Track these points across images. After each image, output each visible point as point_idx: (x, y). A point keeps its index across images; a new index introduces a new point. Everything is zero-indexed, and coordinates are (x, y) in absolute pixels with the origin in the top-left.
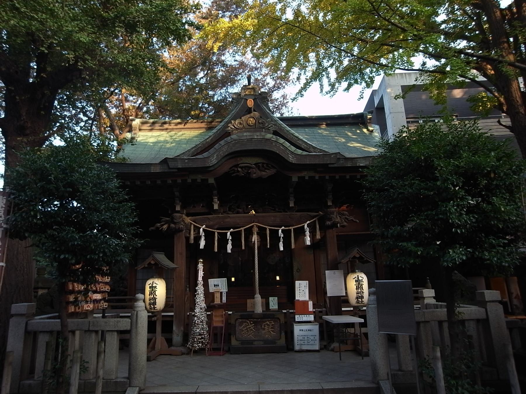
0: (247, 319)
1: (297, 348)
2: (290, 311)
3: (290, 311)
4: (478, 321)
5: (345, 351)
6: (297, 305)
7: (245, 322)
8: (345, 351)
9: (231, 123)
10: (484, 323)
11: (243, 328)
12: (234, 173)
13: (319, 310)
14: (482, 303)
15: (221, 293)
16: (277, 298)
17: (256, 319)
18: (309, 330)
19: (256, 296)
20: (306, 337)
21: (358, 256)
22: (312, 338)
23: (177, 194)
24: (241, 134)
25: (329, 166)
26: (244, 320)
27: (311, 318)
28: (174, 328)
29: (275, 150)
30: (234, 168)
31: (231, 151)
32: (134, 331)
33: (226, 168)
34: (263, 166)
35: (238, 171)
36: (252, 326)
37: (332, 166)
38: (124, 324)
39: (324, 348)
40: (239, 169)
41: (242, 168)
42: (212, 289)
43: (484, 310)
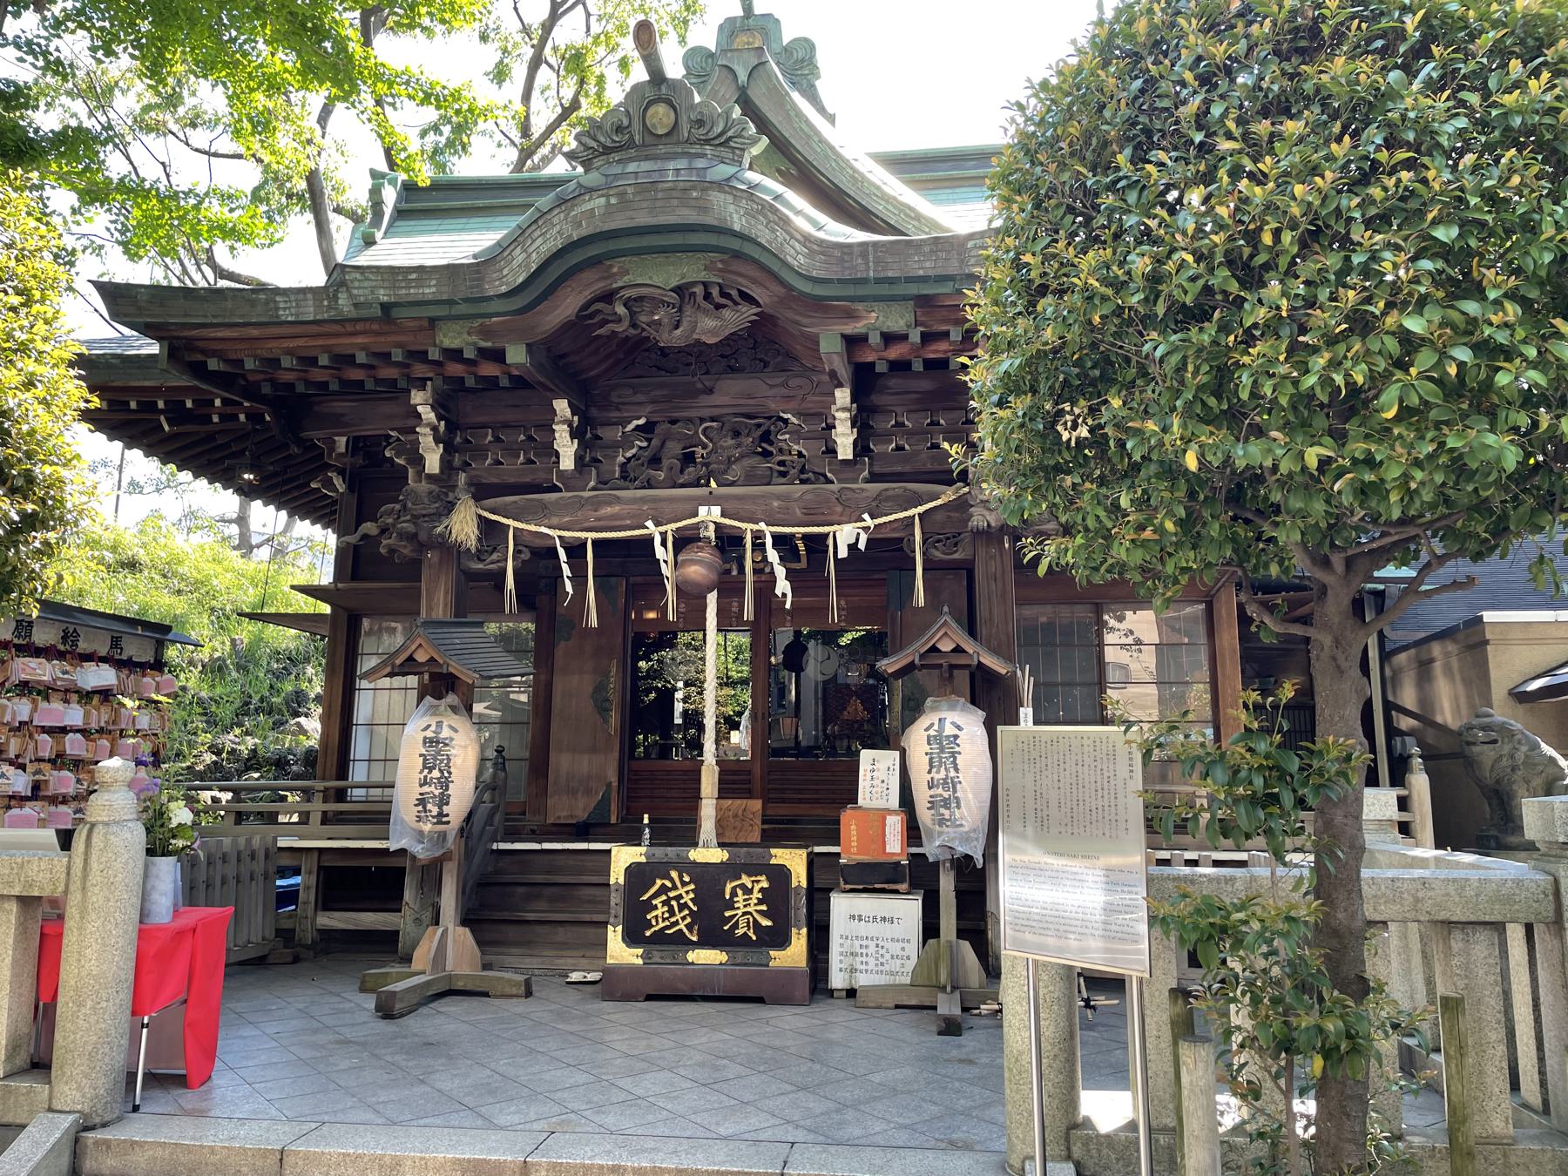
5: (897, 1007)
8: (897, 1007)
11: (655, 896)
18: (883, 919)
20: (872, 945)
22: (895, 948)
24: (617, 169)
34: (707, 296)
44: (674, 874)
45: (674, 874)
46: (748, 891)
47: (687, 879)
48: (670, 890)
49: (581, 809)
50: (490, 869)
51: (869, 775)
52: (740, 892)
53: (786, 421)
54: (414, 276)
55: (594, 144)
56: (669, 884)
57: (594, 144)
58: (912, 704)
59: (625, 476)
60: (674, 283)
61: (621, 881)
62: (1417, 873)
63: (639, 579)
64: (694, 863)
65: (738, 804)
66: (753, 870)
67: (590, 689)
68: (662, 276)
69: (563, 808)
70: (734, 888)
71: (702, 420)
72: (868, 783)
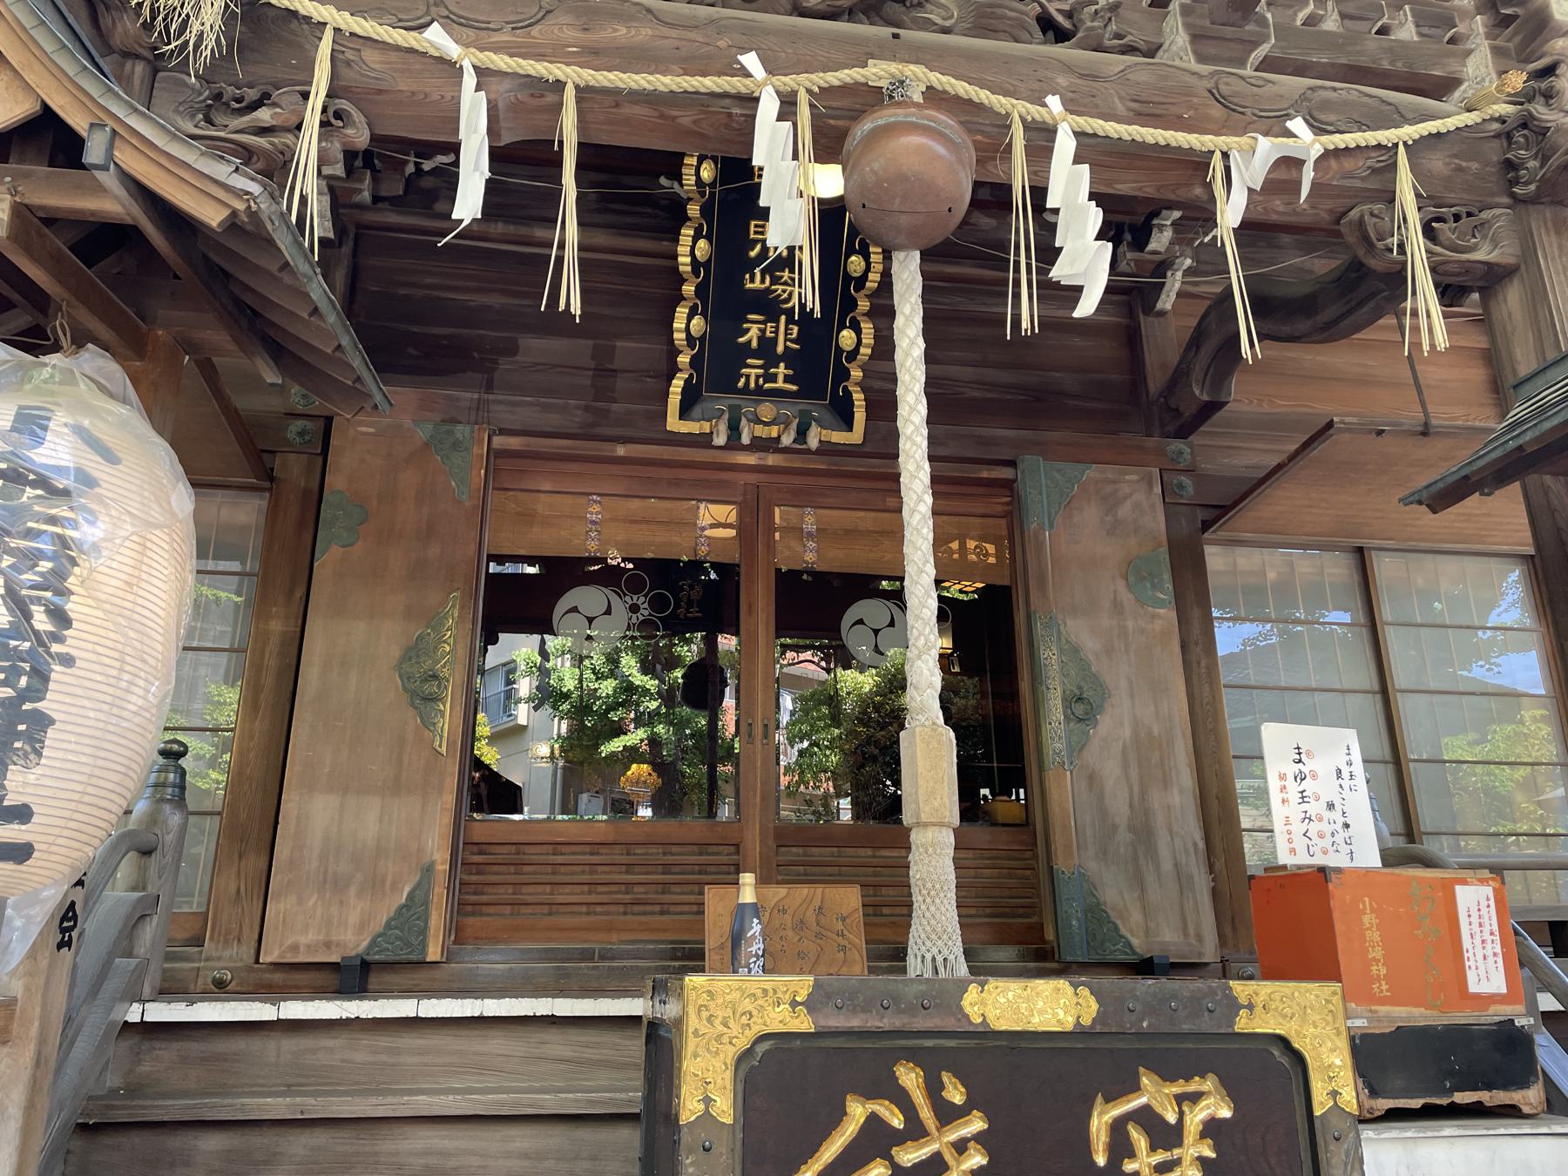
44: (910, 1078)
45: (910, 1078)
46: (1165, 1135)
47: (955, 1094)
48: (901, 1138)
49: (352, 930)
50: (113, 1080)
51: (1293, 788)
52: (1139, 1139)
56: (897, 1122)
58: (1079, 709)
61: (724, 1108)
63: (514, 443)
64: (986, 1034)
66: (1178, 1059)
67: (396, 652)
69: (304, 925)
70: (1118, 1128)
72: (1295, 811)
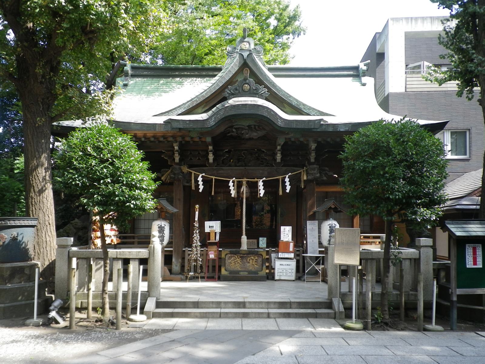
0: (235, 254)
1: (277, 277)
2: (273, 249)
3: (273, 249)
4: (415, 259)
6: (281, 245)
7: (234, 256)
9: (228, 88)
10: (416, 262)
11: (232, 261)
12: (229, 133)
13: (297, 249)
14: (418, 248)
15: (216, 233)
16: (265, 239)
17: (243, 254)
19: (242, 237)
20: (285, 270)
21: (333, 207)
22: (290, 271)
23: (176, 148)
25: (313, 130)
26: (233, 255)
27: (292, 255)
28: (174, 260)
29: (265, 114)
30: (229, 129)
31: (227, 115)
32: (151, 258)
33: (222, 129)
34: (255, 128)
35: (233, 132)
36: (239, 260)
37: (315, 130)
38: (143, 252)
39: (299, 278)
40: (234, 130)
41: (235, 129)
42: (207, 230)
43: (418, 251)
46: (253, 260)
53: (263, 152)
54: (188, 122)
55: (229, 92)
57: (229, 92)
59: (223, 162)
60: (247, 125)
62: (44, 236)
65: (251, 240)
68: (246, 123)
71: (243, 150)
